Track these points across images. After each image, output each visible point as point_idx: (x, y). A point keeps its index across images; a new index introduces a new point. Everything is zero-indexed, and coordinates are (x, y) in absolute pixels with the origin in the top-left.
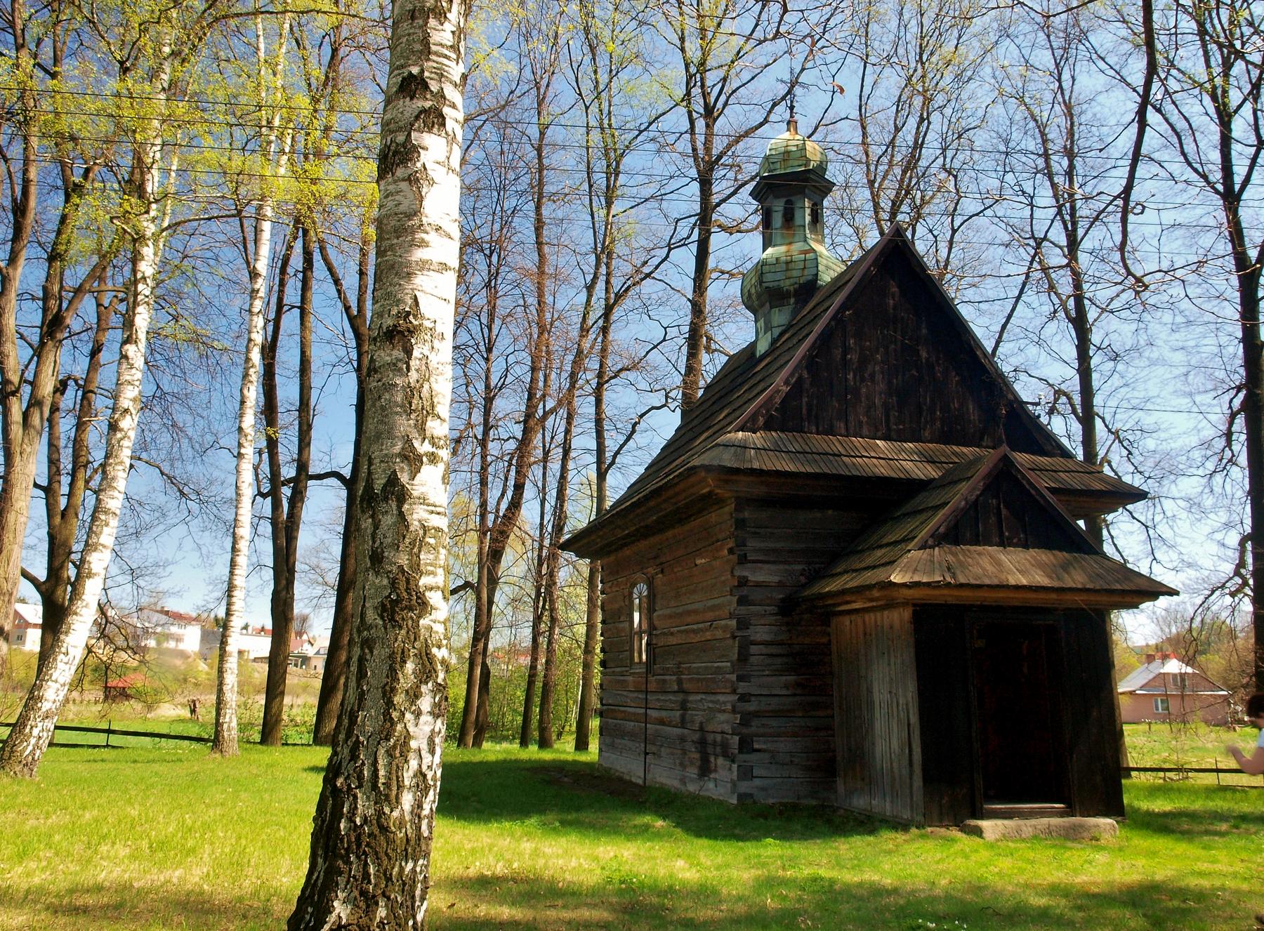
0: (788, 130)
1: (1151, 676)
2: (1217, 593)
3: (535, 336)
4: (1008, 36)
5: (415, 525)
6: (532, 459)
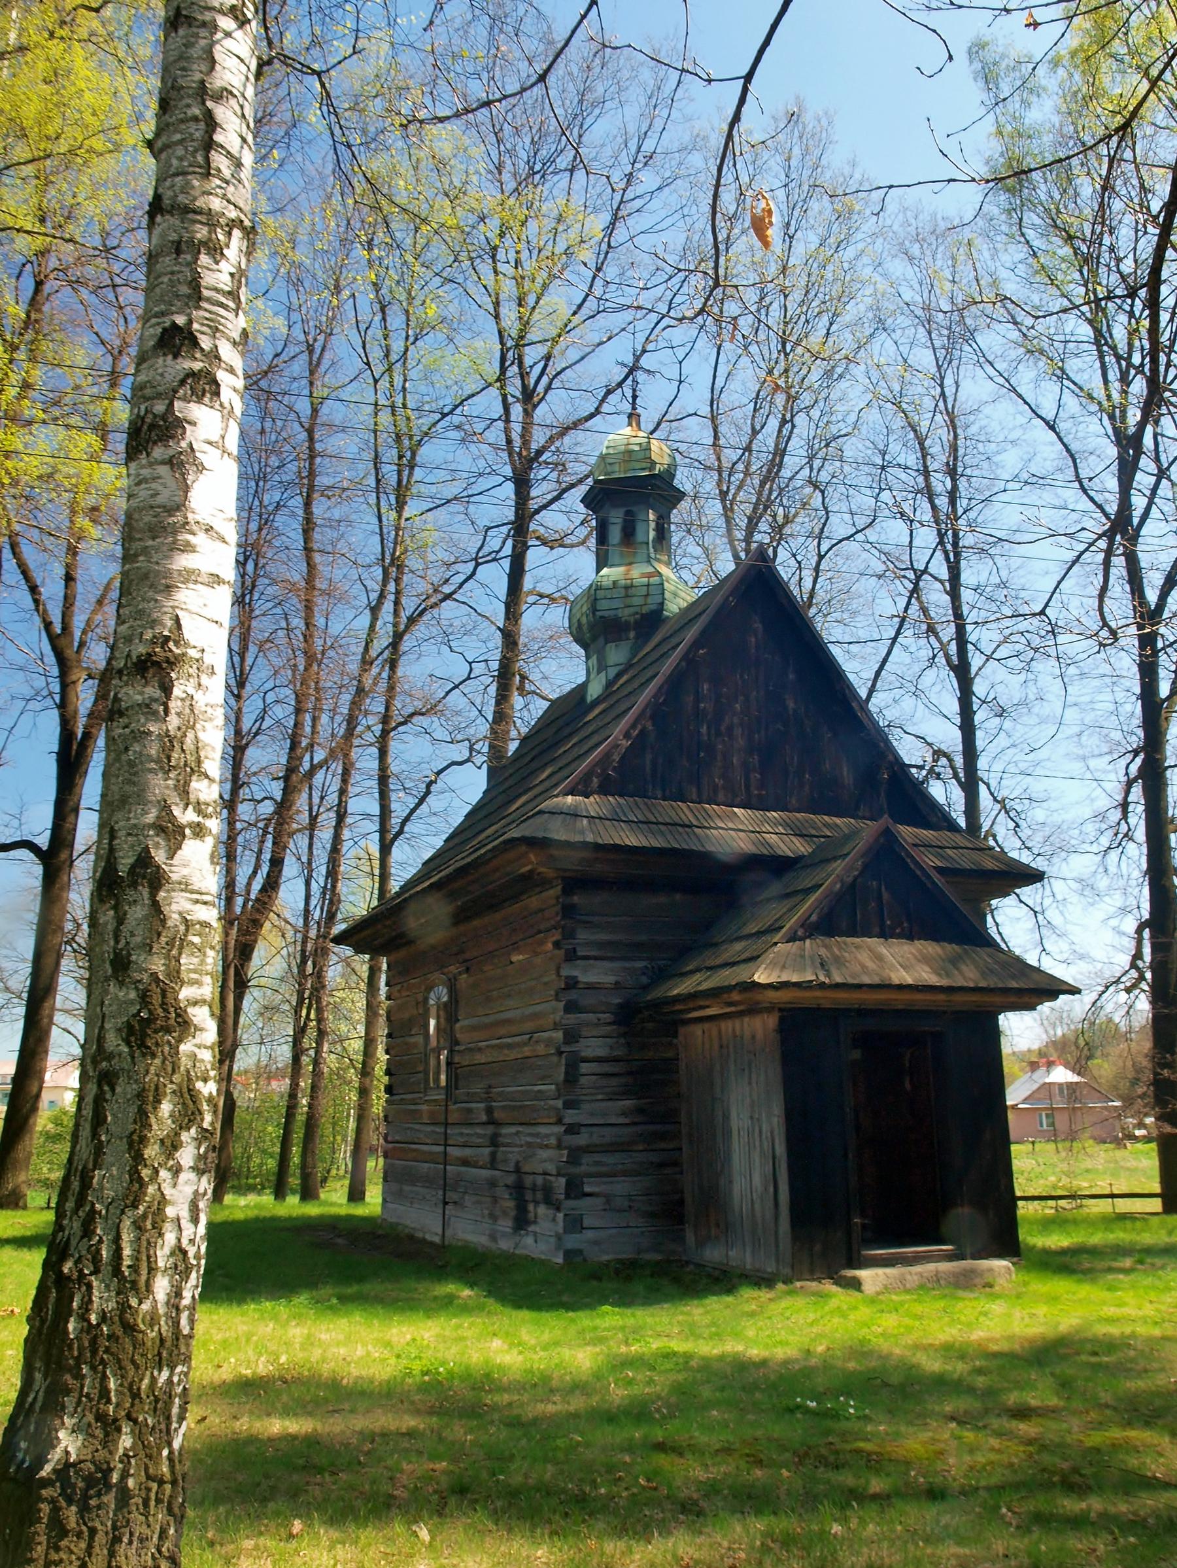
0: (630, 424)
1: (1035, 1086)
2: (1112, 989)
3: (301, 668)
4: (884, 329)
5: (174, 919)
6: (295, 826)
